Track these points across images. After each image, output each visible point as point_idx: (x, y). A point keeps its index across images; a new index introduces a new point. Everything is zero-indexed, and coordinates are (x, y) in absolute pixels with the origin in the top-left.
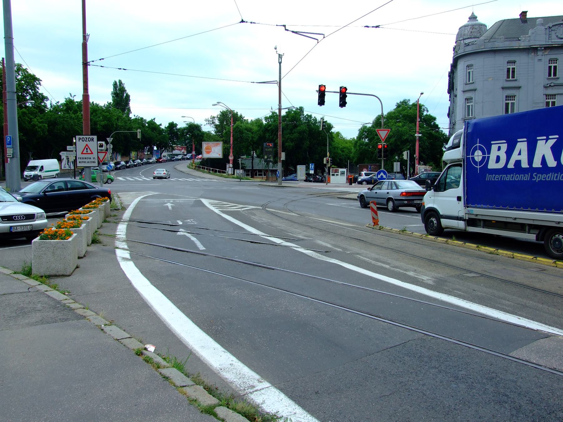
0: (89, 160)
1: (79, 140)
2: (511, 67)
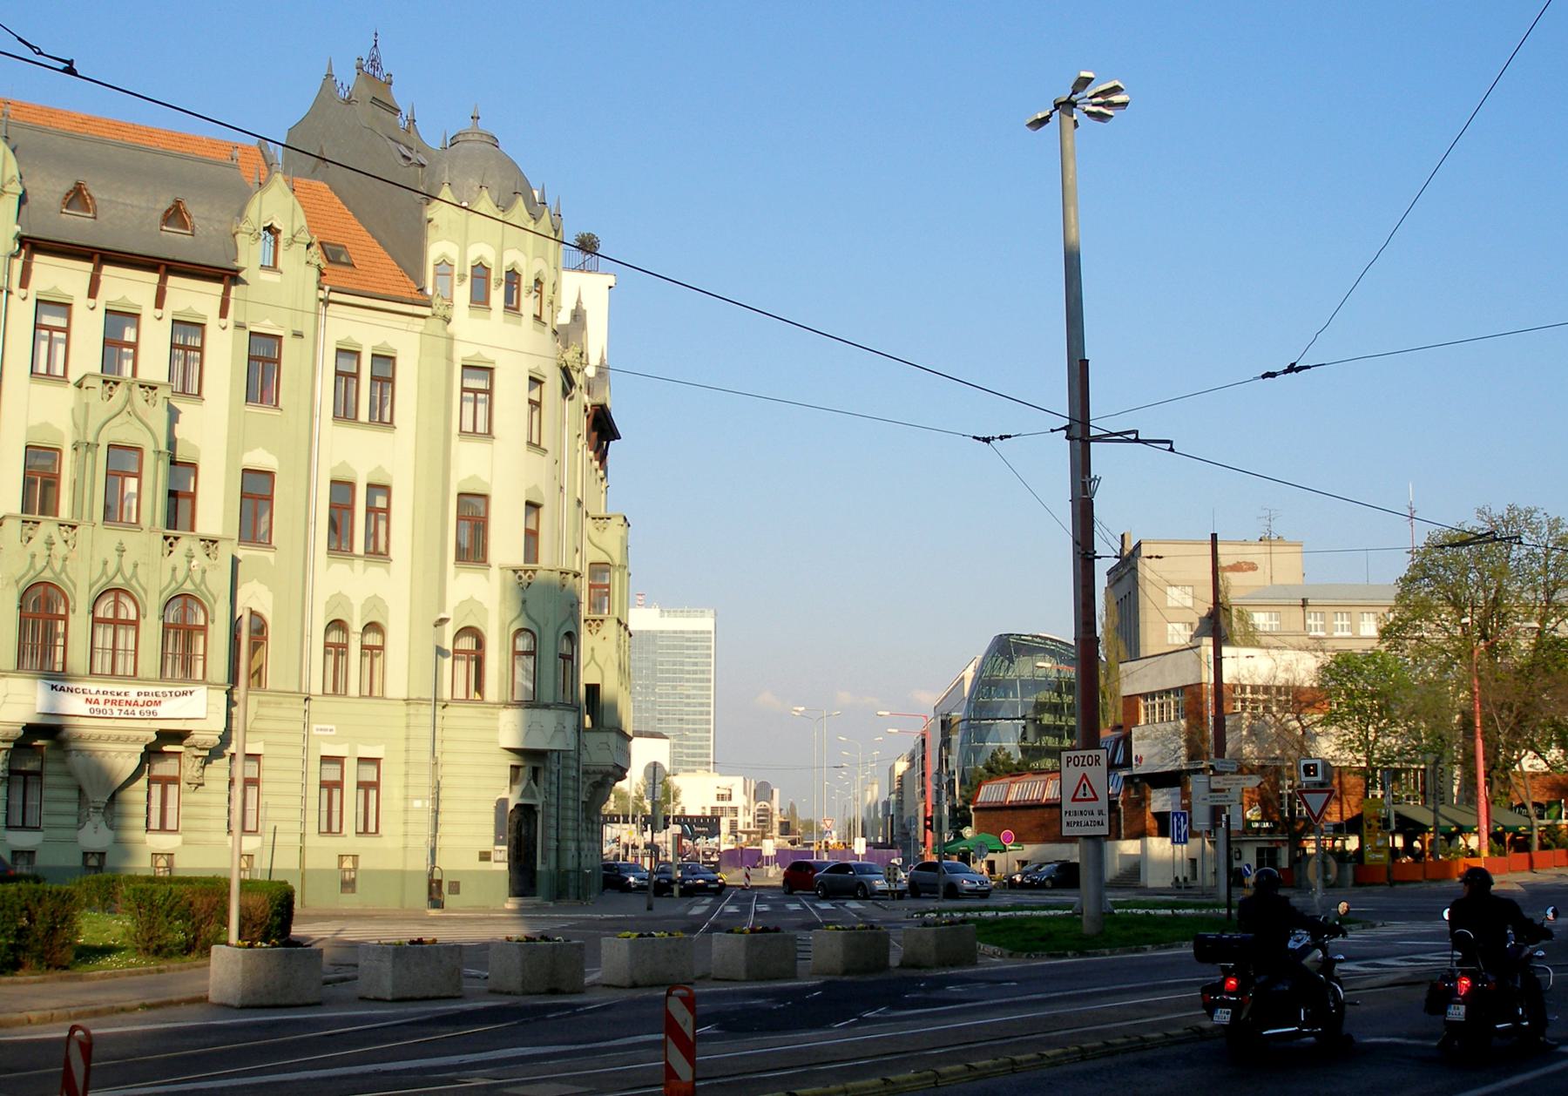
0: (1088, 818)
1: (1068, 762)
2: (349, 842)
